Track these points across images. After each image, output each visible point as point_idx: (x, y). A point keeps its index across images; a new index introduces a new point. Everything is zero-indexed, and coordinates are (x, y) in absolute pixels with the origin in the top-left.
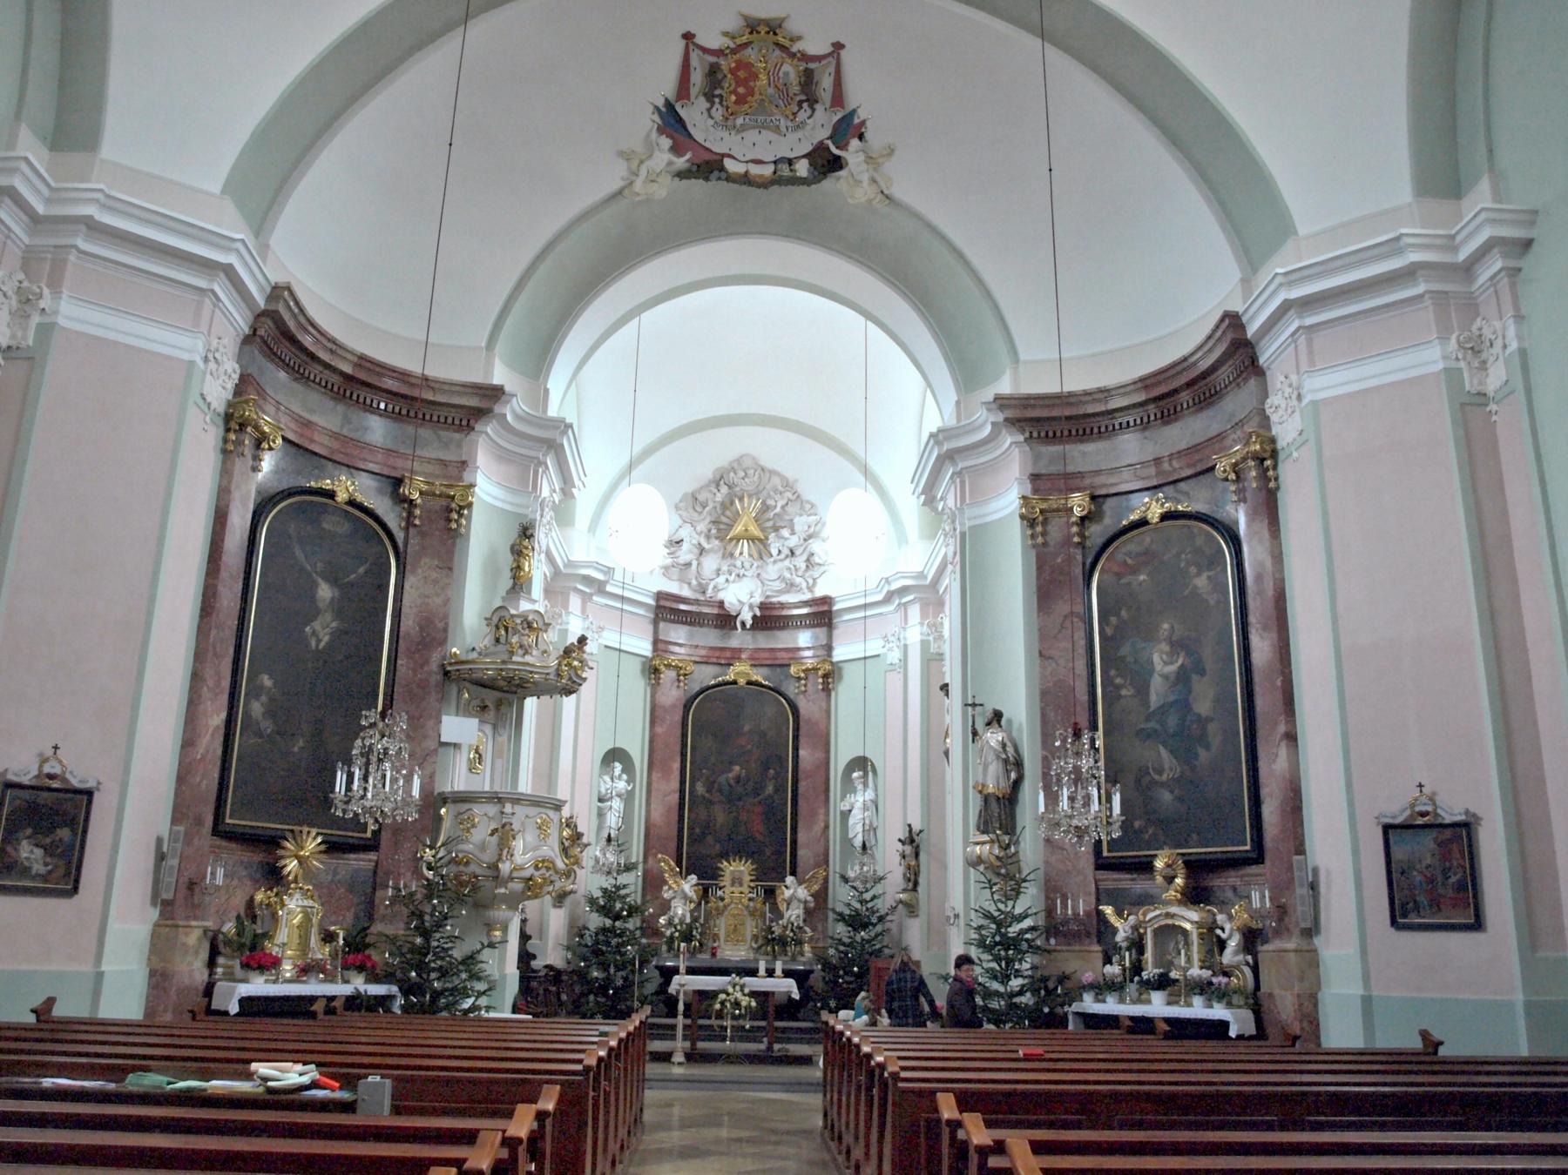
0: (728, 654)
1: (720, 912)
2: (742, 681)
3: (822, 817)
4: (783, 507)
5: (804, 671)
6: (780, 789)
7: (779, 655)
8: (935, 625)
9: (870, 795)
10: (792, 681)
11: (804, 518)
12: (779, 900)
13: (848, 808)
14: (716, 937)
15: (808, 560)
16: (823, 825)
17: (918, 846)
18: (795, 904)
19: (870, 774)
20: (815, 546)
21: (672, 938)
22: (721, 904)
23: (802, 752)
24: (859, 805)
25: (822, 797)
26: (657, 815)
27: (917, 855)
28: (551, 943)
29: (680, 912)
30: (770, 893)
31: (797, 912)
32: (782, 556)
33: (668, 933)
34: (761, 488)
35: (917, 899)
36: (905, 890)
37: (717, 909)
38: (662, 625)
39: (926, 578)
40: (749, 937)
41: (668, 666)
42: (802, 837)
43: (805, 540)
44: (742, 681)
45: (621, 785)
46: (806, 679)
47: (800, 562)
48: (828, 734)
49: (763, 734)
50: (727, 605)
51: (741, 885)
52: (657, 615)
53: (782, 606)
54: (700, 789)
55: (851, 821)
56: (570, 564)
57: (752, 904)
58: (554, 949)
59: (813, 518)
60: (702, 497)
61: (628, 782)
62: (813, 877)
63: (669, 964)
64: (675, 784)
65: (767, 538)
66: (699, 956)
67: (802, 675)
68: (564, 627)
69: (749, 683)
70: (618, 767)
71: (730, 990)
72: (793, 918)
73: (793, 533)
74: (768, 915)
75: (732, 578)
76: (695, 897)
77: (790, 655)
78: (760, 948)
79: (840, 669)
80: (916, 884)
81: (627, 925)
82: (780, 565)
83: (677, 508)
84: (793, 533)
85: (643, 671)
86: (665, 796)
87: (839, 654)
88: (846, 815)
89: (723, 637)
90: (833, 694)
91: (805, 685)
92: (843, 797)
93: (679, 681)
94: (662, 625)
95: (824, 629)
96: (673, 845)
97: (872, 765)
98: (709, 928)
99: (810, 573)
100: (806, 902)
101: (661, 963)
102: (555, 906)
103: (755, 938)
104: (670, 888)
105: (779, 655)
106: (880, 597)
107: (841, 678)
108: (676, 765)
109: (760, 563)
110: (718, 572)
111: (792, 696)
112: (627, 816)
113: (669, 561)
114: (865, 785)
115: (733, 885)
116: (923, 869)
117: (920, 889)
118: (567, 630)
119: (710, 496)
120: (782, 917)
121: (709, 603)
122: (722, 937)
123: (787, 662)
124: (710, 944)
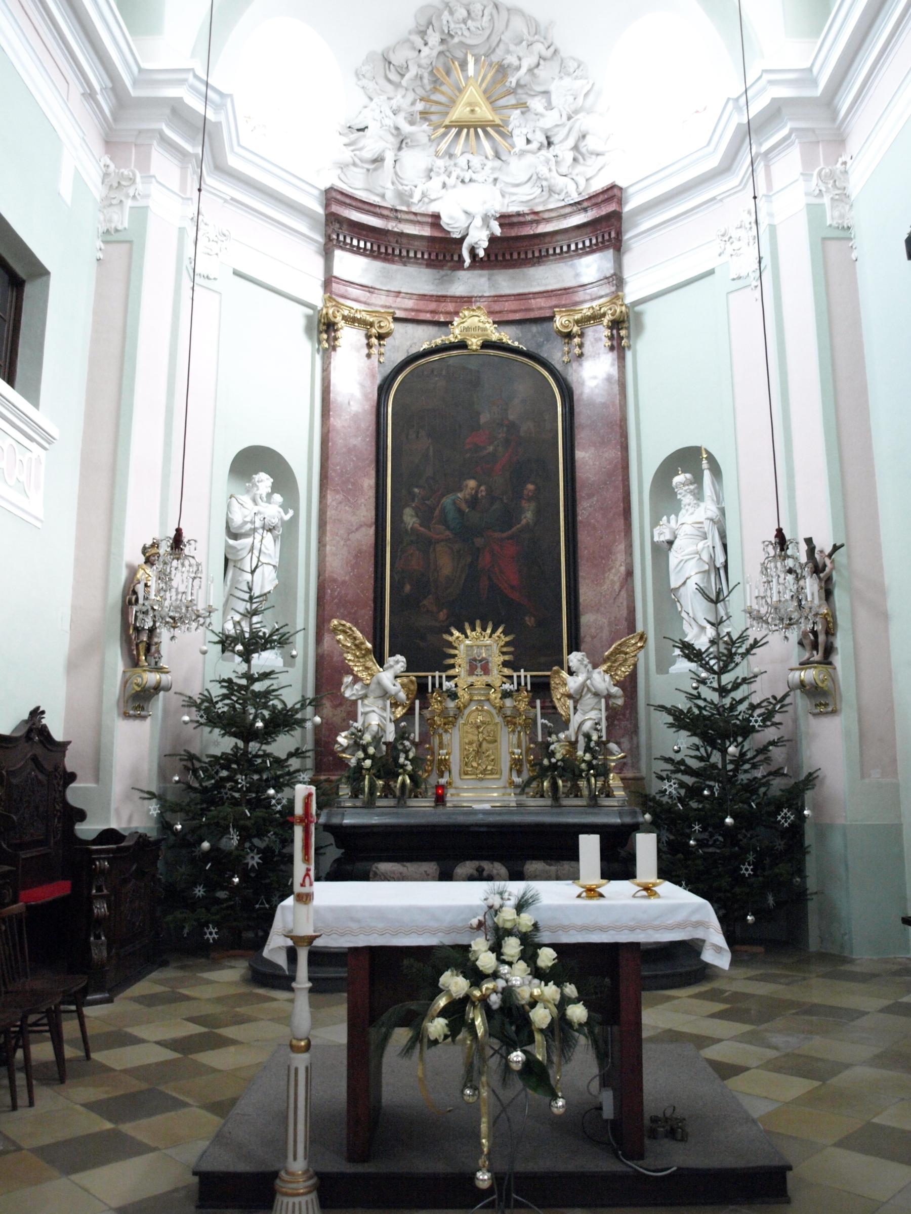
0: (451, 307)
1: (451, 720)
2: (474, 343)
3: (620, 557)
4: (530, 71)
5: (577, 322)
6: (547, 511)
7: (534, 303)
8: (831, 175)
9: (707, 509)
10: (559, 342)
11: (567, 81)
12: (556, 695)
13: (668, 536)
14: (443, 766)
15: (576, 148)
16: (623, 569)
17: (829, 579)
18: (588, 700)
19: (707, 475)
20: (583, 122)
21: (359, 767)
22: (451, 704)
23: (579, 454)
24: (687, 529)
25: (621, 522)
26: (337, 565)
27: (828, 594)
28: (118, 786)
29: (374, 721)
30: (541, 689)
31: (593, 714)
32: (534, 146)
33: (353, 762)
34: (494, 40)
35: (834, 680)
36: (805, 664)
37: (444, 713)
38: (339, 254)
39: (814, 82)
40: (505, 764)
41: (351, 320)
42: (586, 593)
43: (569, 118)
44: (474, 343)
45: (273, 511)
46: (581, 335)
47: (564, 150)
48: (624, 420)
49: (512, 427)
50: (445, 221)
51: (486, 670)
52: (328, 238)
53: (537, 217)
54: (410, 519)
55: (674, 558)
56: (144, 77)
57: (508, 702)
58: (127, 798)
59: (579, 83)
60: (397, 58)
61: (285, 507)
62: (617, 651)
63: (347, 821)
64: (367, 512)
65: (506, 122)
66: (413, 802)
67: (576, 329)
68: (141, 203)
69: (487, 345)
70: (264, 481)
71: (486, 960)
72: (587, 726)
73: (549, 107)
74: (540, 721)
75: (451, 181)
76: (402, 695)
77: (554, 301)
78: (527, 784)
79: (639, 315)
80: (829, 650)
81: (268, 748)
82: (529, 158)
83: (358, 75)
84: (549, 107)
85: (308, 330)
86: (350, 532)
87: (632, 293)
88: (662, 550)
89: (442, 281)
90: (629, 355)
91: (581, 346)
92: (655, 523)
93: (369, 346)
94: (339, 254)
95: (610, 253)
96: (367, 613)
97: (711, 459)
98: (432, 751)
99: (579, 169)
100: (609, 697)
101: (335, 821)
102: (126, 716)
103: (517, 765)
104: (357, 679)
105: (534, 303)
106: (713, 162)
107: (640, 327)
108: (369, 482)
109: (498, 163)
110: (429, 173)
111: (559, 367)
112: (285, 569)
113: (347, 155)
114: (699, 496)
115: (471, 671)
116: (842, 620)
117: (838, 660)
118: (146, 208)
119: (413, 54)
120: (565, 724)
121: (416, 218)
122: (455, 766)
123: (548, 314)
124: (433, 780)
